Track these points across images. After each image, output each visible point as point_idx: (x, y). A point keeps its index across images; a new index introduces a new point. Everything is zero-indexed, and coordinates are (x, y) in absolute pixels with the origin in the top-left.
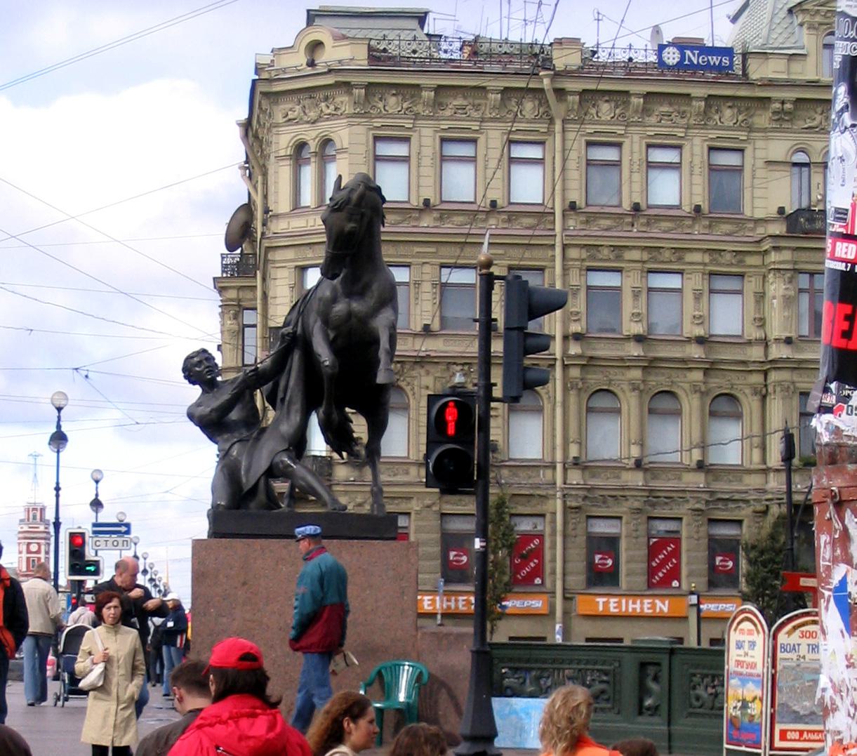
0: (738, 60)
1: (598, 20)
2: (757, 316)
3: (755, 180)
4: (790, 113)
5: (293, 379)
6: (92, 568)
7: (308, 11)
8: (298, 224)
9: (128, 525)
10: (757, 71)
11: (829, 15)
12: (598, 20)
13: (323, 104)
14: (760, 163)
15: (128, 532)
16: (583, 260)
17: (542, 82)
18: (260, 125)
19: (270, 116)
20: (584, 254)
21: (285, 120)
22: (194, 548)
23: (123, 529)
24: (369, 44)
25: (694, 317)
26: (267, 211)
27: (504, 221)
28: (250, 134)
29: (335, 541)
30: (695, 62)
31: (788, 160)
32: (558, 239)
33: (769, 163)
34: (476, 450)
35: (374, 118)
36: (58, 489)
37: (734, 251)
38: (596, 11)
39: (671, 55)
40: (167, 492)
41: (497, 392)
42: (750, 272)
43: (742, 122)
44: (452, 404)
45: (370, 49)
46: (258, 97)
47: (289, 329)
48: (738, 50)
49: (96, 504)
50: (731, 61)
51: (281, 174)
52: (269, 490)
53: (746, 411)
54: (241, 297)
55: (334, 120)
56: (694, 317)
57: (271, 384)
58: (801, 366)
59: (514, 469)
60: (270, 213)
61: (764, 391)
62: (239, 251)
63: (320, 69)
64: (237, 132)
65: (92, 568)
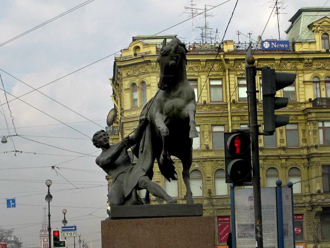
0: (290, 45)
1: (239, 34)
2: (304, 138)
3: (300, 89)
4: (311, 63)
5: (146, 142)
6: (62, 244)
7: (133, 38)
8: (134, 113)
9: (75, 227)
10: (298, 48)
11: (323, 27)
12: (239, 34)
13: (141, 69)
14: (301, 82)
15: (75, 230)
16: (239, 121)
17: (220, 57)
18: (118, 79)
19: (121, 75)
20: (239, 119)
21: (127, 75)
22: (102, 225)
23: (74, 228)
24: (156, 46)
25: (281, 139)
26: (122, 109)
27: (209, 108)
28: (115, 83)
29: (172, 218)
30: (275, 47)
31: (311, 80)
32: (229, 114)
33: (304, 82)
34: (252, 163)
35: (282, 71)
36: (49, 216)
37: (294, 115)
38: (237, 31)
39: (266, 45)
40: (90, 215)
41: (261, 129)
42: (300, 122)
43: (294, 67)
44: (237, 138)
45: (156, 48)
46: (116, 68)
47: (144, 117)
48: (291, 41)
49: (65, 221)
50: (288, 46)
51: (127, 97)
52: (137, 197)
53: (302, 174)
54: (113, 142)
55: (145, 74)
56: (281, 139)
57: (135, 145)
58: (321, 156)
59: (218, 200)
60: (123, 110)
61: (308, 166)
62: (112, 126)
63: (138, 57)
64: (111, 82)
65: (62, 244)
